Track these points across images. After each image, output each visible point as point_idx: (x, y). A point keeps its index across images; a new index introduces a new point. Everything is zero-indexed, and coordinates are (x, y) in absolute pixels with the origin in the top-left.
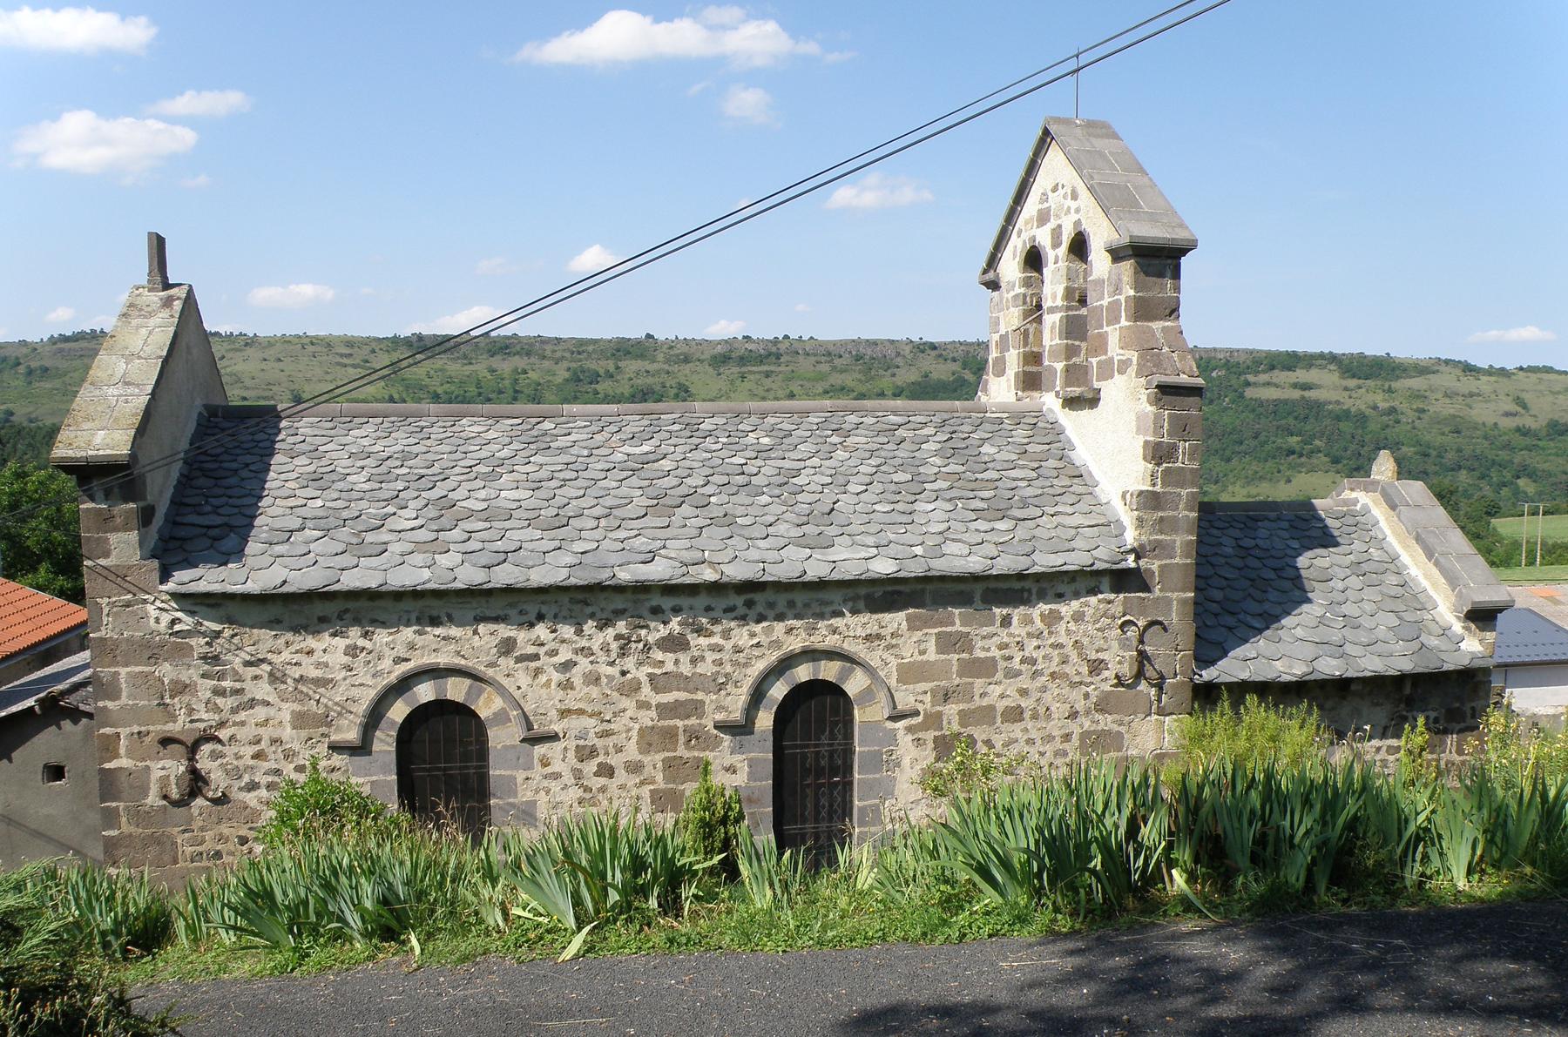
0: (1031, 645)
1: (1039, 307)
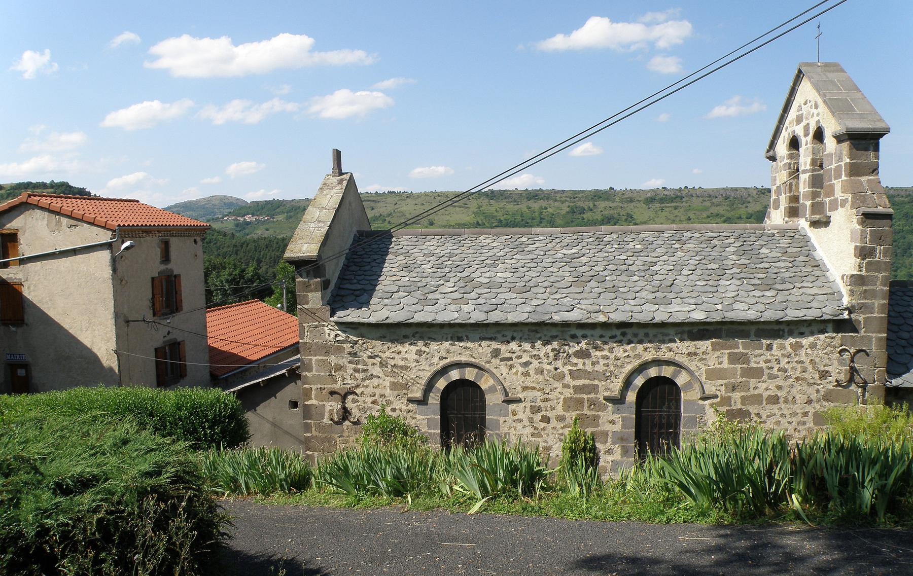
1: (798, 170)
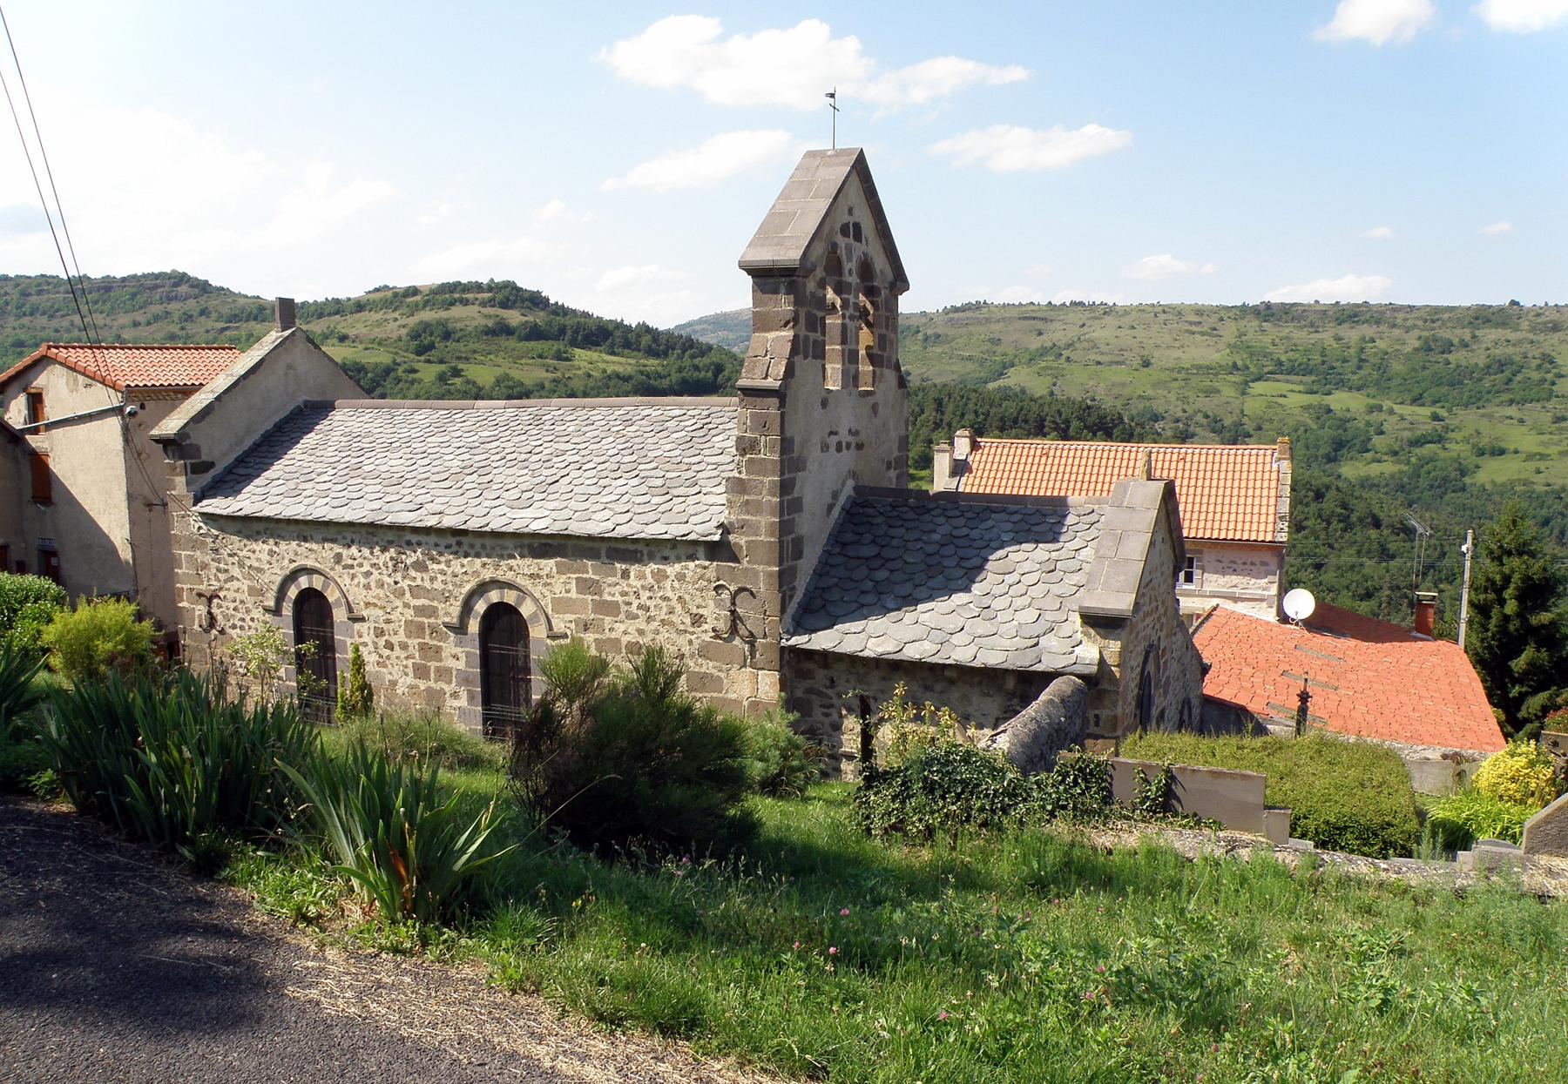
0: (645, 595)
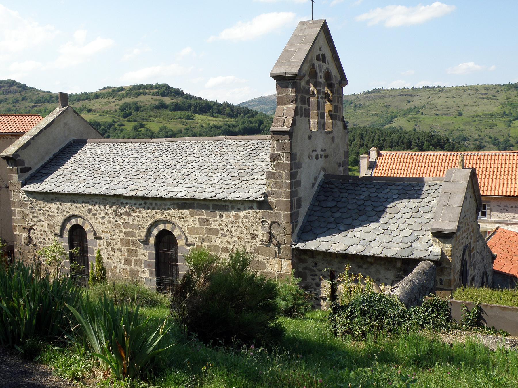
0: (230, 225)
